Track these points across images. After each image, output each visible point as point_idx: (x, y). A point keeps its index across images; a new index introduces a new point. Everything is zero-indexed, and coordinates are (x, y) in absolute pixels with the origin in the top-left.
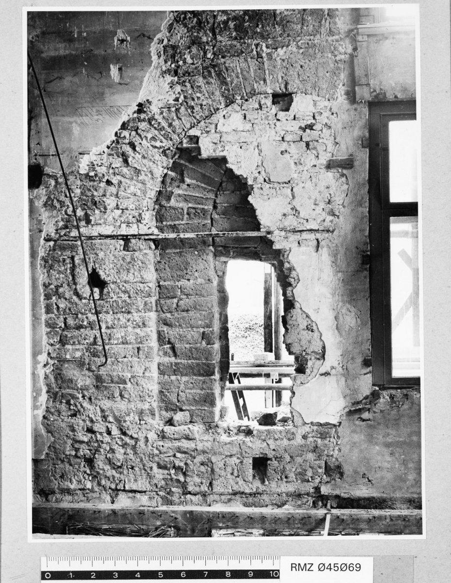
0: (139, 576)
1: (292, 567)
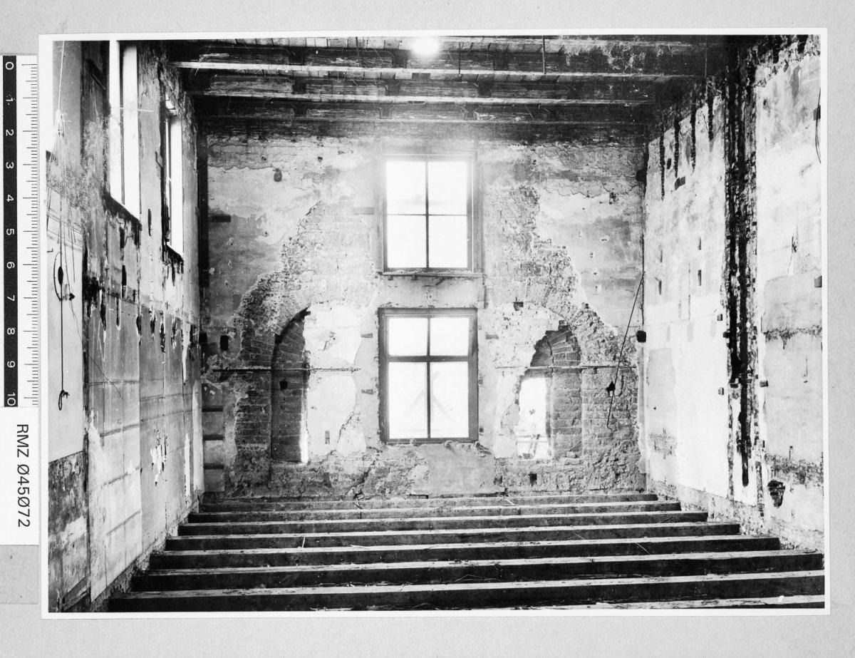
0: (8, 200)
1: (23, 426)
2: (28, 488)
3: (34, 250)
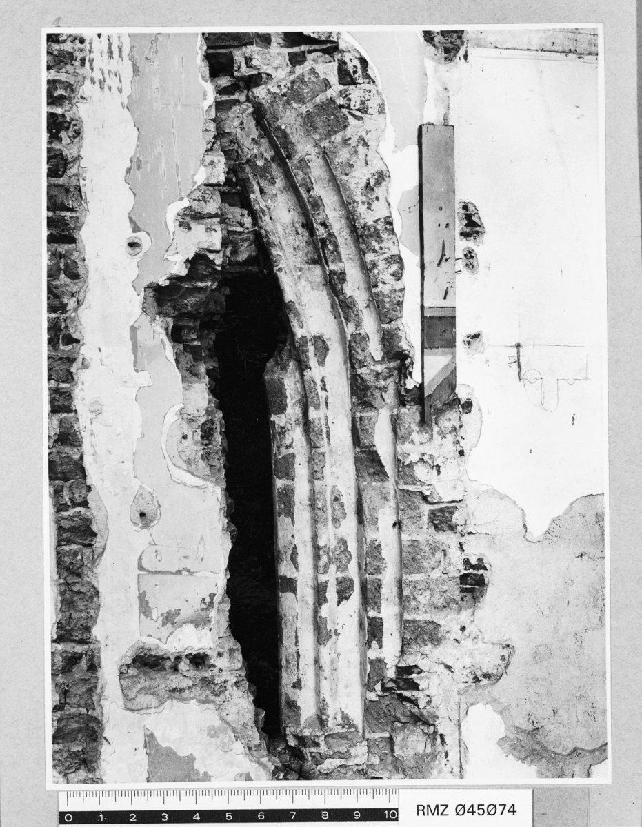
0: (198, 818)
1: (418, 810)
2: (479, 805)
3: (246, 793)
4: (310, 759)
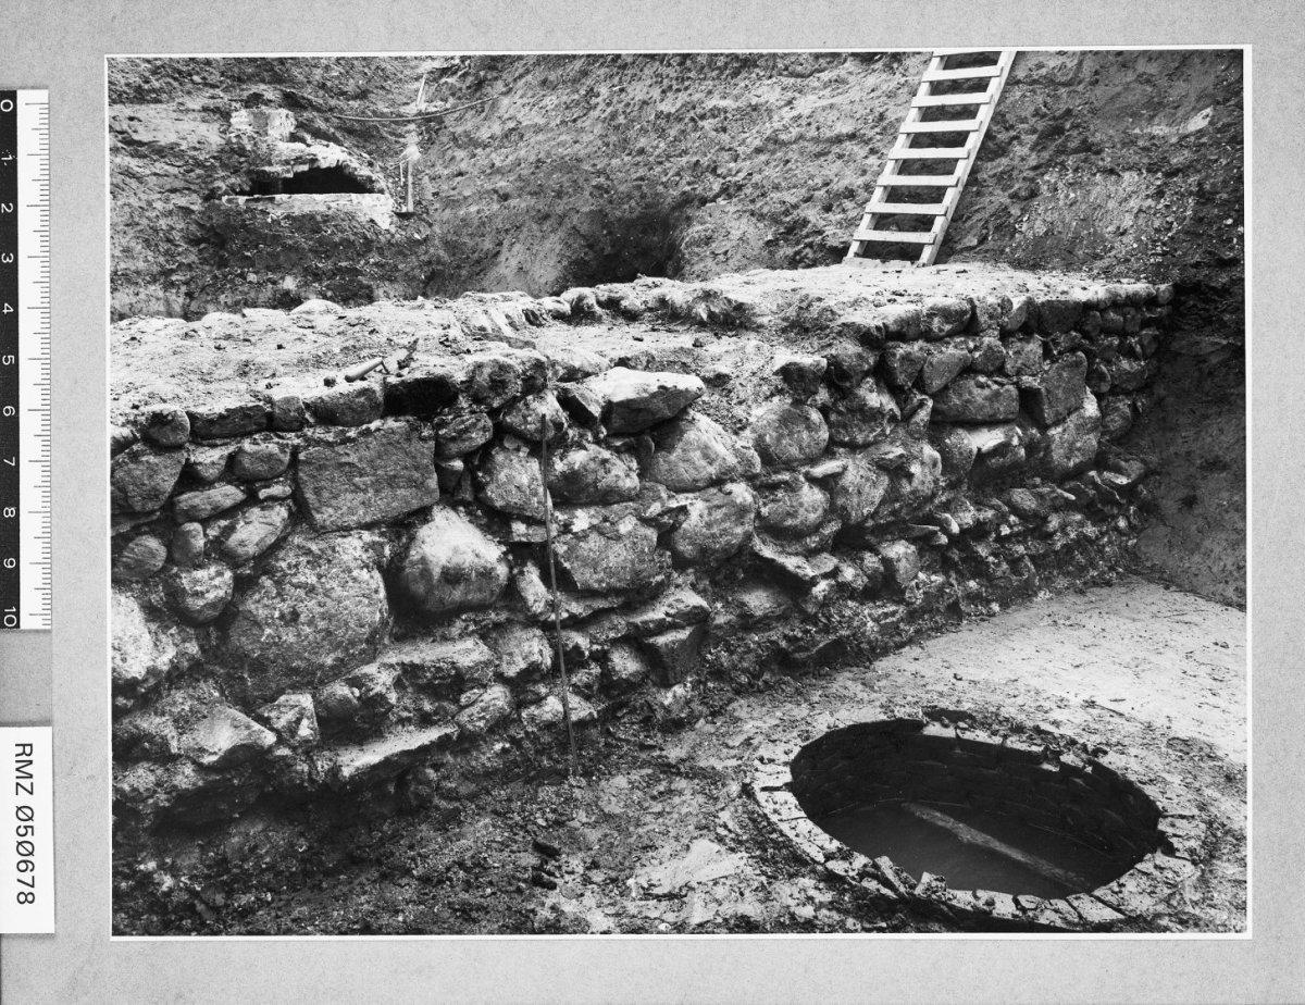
1: (24, 745)
4: (673, 504)
